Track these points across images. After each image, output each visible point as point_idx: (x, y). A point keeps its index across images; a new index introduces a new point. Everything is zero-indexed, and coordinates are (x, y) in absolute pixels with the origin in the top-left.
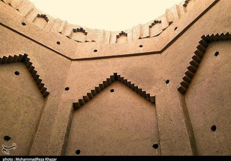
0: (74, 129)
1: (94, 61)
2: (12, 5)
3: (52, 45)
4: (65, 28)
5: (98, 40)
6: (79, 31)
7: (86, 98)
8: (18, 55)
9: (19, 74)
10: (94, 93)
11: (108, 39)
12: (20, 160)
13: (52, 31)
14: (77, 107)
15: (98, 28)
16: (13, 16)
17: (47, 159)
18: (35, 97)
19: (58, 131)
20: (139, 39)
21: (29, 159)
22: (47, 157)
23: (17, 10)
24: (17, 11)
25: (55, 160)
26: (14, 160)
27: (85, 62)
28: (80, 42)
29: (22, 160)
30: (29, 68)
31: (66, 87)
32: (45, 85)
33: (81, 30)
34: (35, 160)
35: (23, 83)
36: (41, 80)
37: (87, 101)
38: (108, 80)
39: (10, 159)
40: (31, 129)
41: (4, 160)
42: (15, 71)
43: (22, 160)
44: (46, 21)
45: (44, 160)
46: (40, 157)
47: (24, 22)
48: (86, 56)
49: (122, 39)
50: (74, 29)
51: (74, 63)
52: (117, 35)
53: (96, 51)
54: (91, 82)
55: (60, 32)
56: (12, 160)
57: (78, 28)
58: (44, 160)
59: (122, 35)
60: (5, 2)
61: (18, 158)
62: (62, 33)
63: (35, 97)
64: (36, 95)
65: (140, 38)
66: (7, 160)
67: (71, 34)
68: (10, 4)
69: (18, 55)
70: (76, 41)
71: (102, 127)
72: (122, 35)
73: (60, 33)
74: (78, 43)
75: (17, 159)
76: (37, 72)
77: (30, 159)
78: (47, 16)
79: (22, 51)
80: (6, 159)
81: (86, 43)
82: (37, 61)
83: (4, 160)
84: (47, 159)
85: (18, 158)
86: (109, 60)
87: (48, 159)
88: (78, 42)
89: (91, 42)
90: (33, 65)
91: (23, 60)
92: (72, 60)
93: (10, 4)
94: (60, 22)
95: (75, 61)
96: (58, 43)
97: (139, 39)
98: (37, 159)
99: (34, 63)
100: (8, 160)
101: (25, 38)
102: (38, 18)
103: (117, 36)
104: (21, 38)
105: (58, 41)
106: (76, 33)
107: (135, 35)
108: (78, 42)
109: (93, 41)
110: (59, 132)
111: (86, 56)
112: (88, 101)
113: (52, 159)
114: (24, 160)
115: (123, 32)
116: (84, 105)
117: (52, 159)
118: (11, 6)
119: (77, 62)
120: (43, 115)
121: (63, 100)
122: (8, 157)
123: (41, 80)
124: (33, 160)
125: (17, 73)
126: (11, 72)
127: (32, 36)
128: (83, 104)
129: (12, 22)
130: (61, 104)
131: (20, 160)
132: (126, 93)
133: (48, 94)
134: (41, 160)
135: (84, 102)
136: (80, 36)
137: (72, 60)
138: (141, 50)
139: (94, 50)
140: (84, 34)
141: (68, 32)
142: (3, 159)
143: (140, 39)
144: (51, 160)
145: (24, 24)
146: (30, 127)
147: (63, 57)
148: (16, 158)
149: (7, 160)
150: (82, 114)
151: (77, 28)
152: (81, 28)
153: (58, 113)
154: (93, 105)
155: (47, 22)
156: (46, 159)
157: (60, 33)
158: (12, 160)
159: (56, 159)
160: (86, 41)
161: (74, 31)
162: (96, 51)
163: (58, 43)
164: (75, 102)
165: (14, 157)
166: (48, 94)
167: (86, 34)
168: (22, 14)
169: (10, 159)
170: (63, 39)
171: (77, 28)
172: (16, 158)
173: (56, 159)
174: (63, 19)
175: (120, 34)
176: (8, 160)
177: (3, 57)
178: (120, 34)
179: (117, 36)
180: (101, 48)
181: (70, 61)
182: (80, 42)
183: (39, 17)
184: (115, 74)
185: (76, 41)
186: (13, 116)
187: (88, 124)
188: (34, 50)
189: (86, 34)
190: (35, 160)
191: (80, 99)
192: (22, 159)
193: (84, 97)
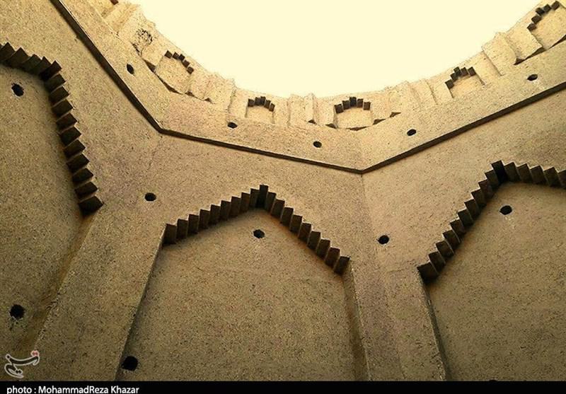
0: (451, 331)
1: (420, 157)
2: (194, 93)
3: (309, 153)
4: (316, 110)
5: (404, 105)
6: (348, 108)
7: (443, 246)
8: (249, 192)
9: (263, 234)
10: (460, 230)
11: (429, 96)
12: (49, 391)
13: (293, 123)
14: (431, 274)
15: (393, 83)
16: (205, 116)
17: (115, 389)
18: (318, 278)
19: (413, 346)
20: (515, 64)
21: (70, 390)
22: (114, 384)
23: (208, 100)
24: (209, 103)
25: (134, 390)
26: (33, 391)
27: (396, 167)
28: (361, 128)
29: (55, 390)
30: (279, 217)
31: (379, 236)
32: (331, 244)
33: (353, 103)
34: (86, 391)
35: (278, 250)
36: (319, 234)
37: (449, 253)
38: (484, 185)
39: (25, 388)
40: (344, 356)
41: (10, 391)
42: (253, 230)
43: (55, 390)
44: (270, 110)
45: (107, 391)
46: (97, 384)
47: (231, 121)
48: (392, 153)
49: (465, 85)
50: (335, 106)
51: (366, 177)
52: (474, 68)
53: (412, 132)
54: (441, 205)
55: (310, 122)
56: (29, 391)
57: (345, 100)
58: (107, 391)
59: (459, 78)
60: (178, 91)
61: (45, 387)
62: (315, 121)
63: (318, 278)
64: (320, 275)
65: (519, 62)
66: (18, 391)
67: (336, 119)
68: (189, 94)
69: (249, 192)
70: (351, 129)
71: (529, 307)
72: (459, 78)
73: (312, 121)
74: (359, 131)
75: (41, 390)
76: (302, 217)
77: (75, 390)
78: (267, 99)
79: (255, 181)
80: (14, 389)
81: (376, 125)
82: (291, 196)
83: (10, 391)
84: (115, 389)
85: (45, 387)
86: (463, 140)
87: (118, 389)
88: (357, 129)
89: (390, 119)
90: (288, 205)
91: (261, 202)
92: (361, 173)
93: (189, 94)
94: (301, 101)
95: (371, 173)
96: (317, 144)
97: (515, 64)
98: (90, 389)
99: (287, 200)
100: (20, 391)
101: (247, 154)
102: (252, 108)
103: (446, 83)
104: (238, 155)
105: (314, 141)
106: (342, 114)
107: (500, 63)
108: (357, 129)
109: (393, 114)
110: (419, 348)
111: (392, 153)
112: (452, 255)
113: (127, 390)
114: (60, 391)
115: (458, 68)
116: (446, 267)
117: (127, 390)
118: (193, 96)
119: (376, 174)
120: (360, 313)
121: (389, 268)
122: (19, 384)
123: (319, 234)
124: (82, 391)
125: (259, 234)
126: (245, 235)
127: (258, 144)
128: (443, 265)
129: (208, 127)
130: (387, 281)
131: (49, 391)
132: (550, 204)
133: (346, 261)
134: (101, 392)
135: (442, 259)
136: (354, 117)
137: (361, 173)
138: (539, 86)
139: (408, 133)
140: (362, 109)
141: (328, 116)
142: (8, 389)
143: (519, 65)
144: (124, 391)
145: (232, 125)
146: (339, 351)
147: (340, 172)
148: (40, 387)
149: (18, 391)
150: (453, 286)
151: (343, 102)
152: (350, 98)
153: (391, 301)
154: (470, 259)
155: (272, 110)
156: (113, 389)
157: (312, 121)
158: (29, 391)
159: (137, 389)
160: (377, 122)
161: (339, 109)
162: (412, 132)
163: (317, 144)
164: (422, 264)
165: (34, 385)
166: (346, 261)
167: (367, 106)
168: (219, 106)
169: (25, 388)
170: (323, 133)
171: (343, 102)
172: (40, 387)
173: (137, 389)
174: (302, 92)
175: (452, 76)
176: (20, 391)
177: (176, 222)
178: (452, 76)
179: (446, 83)
180: (422, 121)
181: (358, 176)
182: (361, 128)
183: (252, 106)
184: (498, 166)
185: (351, 129)
186: (291, 333)
187: (485, 310)
188: (275, 173)
189: (367, 106)
190: (86, 391)
191: (431, 252)
192: (53, 389)
193: (439, 245)
